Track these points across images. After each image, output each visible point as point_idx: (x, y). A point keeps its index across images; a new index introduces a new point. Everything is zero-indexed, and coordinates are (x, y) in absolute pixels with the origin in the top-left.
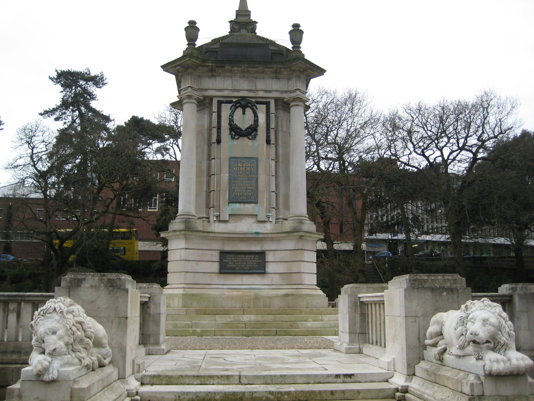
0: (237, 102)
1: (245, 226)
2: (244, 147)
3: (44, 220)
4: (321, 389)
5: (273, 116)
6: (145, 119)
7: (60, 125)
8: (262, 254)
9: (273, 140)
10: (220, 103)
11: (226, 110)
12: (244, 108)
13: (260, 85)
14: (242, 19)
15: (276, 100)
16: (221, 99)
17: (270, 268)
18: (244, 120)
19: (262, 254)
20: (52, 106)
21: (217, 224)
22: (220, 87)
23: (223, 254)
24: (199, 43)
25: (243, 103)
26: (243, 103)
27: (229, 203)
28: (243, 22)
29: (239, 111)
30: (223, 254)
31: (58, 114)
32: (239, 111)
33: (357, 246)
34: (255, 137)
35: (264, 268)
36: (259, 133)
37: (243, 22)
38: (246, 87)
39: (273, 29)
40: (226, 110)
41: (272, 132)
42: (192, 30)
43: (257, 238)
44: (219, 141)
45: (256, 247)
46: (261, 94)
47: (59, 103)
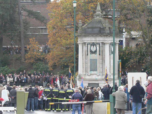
0: (92, 44)
1: (94, 77)
2: (94, 56)
3: (53, 93)
4: (106, 58)
5: (101, 48)
9: (101, 54)
10: (88, 44)
11: (89, 45)
12: (93, 46)
15: (102, 43)
16: (88, 43)
18: (93, 49)
19: (98, 84)
21: (87, 76)
22: (88, 40)
25: (93, 44)
26: (93, 44)
27: (90, 71)
29: (92, 46)
30: (97, 60)
32: (92, 46)
38: (94, 40)
40: (89, 45)
41: (101, 52)
43: (96, 80)
44: (88, 55)
45: (97, 82)
46: (98, 41)
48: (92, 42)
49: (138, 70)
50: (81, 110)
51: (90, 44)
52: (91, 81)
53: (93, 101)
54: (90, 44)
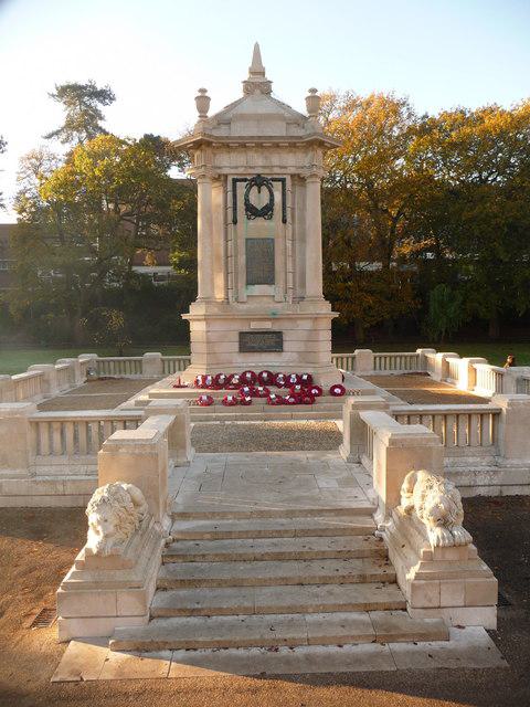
0: (252, 180)
2: (259, 227)
5: (289, 195)
7: (67, 148)
8: (279, 334)
10: (235, 181)
11: (241, 187)
14: (258, 79)
15: (292, 176)
17: (286, 346)
19: (279, 334)
20: (56, 129)
23: (242, 334)
24: (211, 113)
25: (258, 181)
28: (258, 85)
29: (255, 189)
31: (64, 136)
32: (255, 189)
33: (386, 266)
34: (270, 218)
36: (275, 213)
37: (258, 85)
40: (241, 187)
42: (203, 101)
43: (274, 318)
44: (235, 222)
46: (276, 170)
47: (63, 124)
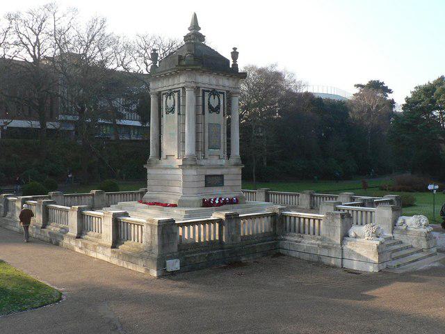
6: (431, 82)
10: (204, 91)
11: (207, 94)
13: (221, 82)
17: (226, 183)
19: (222, 176)
23: (206, 176)
25: (214, 93)
30: (206, 176)
35: (223, 183)
37: (195, 37)
39: (218, 42)
40: (207, 94)
44: (204, 113)
48: (211, 87)
49: (244, 135)
50: (51, 117)
51: (208, 91)
52: (232, 147)
53: (124, 264)
54: (208, 91)
